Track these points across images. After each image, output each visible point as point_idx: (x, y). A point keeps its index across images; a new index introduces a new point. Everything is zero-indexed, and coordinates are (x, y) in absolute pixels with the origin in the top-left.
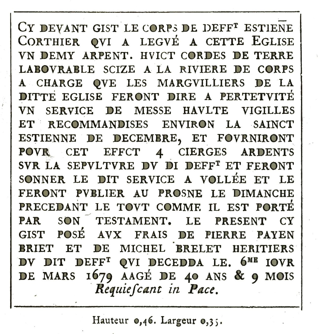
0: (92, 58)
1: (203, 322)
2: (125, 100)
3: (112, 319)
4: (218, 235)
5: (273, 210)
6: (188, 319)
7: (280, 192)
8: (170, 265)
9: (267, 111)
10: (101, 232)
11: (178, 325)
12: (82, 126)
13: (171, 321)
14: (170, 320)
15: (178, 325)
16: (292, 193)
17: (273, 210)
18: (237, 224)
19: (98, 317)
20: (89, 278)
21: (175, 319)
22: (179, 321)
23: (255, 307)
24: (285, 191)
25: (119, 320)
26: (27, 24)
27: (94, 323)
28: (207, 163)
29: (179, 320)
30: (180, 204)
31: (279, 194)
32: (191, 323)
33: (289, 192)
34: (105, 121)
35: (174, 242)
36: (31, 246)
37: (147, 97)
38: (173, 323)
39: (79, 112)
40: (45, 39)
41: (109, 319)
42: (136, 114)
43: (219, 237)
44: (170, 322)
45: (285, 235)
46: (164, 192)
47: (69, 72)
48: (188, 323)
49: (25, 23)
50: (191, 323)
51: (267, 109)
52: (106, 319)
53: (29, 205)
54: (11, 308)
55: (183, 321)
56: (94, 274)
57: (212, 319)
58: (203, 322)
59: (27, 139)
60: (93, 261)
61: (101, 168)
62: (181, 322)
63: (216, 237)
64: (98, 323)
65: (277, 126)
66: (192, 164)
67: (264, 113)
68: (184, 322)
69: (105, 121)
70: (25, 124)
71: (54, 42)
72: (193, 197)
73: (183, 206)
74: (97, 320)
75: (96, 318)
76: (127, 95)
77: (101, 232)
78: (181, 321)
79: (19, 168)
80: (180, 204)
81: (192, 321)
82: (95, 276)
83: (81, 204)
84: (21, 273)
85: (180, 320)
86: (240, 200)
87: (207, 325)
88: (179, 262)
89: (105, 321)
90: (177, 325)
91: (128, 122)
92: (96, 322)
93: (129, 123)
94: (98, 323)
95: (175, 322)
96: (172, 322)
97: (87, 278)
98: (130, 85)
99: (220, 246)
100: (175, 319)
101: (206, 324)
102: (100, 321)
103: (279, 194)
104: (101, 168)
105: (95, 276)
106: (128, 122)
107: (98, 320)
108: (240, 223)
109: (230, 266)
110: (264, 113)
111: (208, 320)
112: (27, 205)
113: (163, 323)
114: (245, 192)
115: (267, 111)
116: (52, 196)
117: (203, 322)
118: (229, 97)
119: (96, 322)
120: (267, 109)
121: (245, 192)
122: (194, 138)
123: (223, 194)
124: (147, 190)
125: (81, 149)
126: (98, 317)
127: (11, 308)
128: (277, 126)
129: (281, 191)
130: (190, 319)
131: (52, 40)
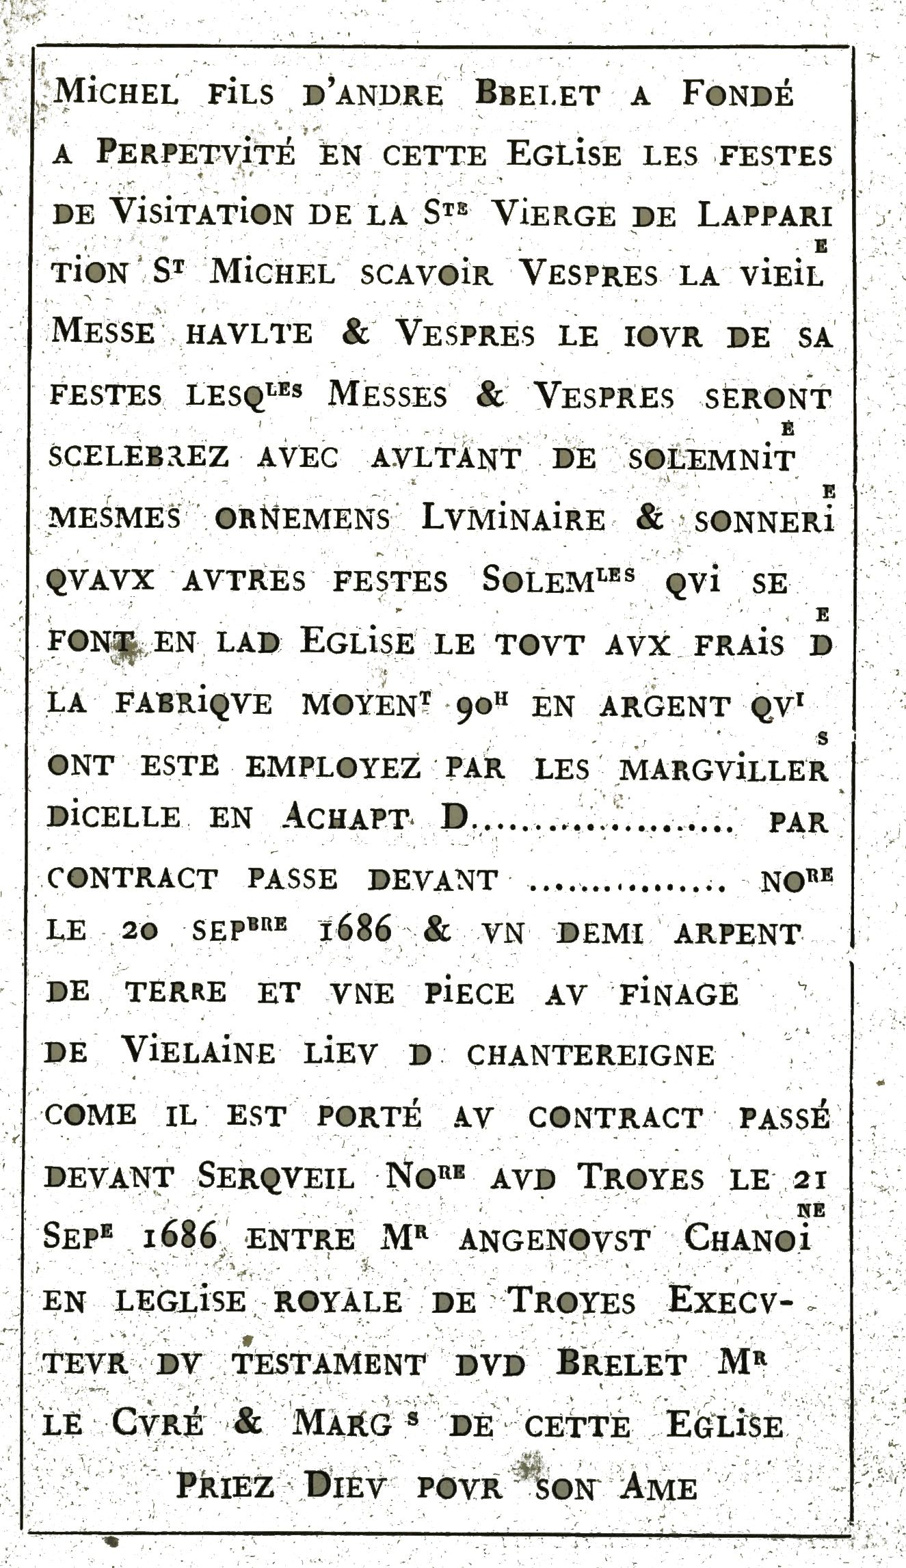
4: (146, 94)
5: (364, 1125)
7: (119, 89)
10: (501, 1172)
12: (94, 1120)
16: (199, 455)
17: (364, 1125)
24: (290, 267)
31: (327, 822)
33: (150, 514)
43: (150, 98)
45: (378, 1364)
61: (266, 341)
66: (65, 987)
76: (231, 926)
77: (501, 1172)
79: (754, 590)
83: (597, 1110)
84: (374, 872)
86: (588, 1394)
98: (226, 646)
103: (326, 820)
104: (266, 341)
118: (185, 154)
122: (234, 1115)
123: (776, 1427)
124: (638, 926)
129: (123, 87)
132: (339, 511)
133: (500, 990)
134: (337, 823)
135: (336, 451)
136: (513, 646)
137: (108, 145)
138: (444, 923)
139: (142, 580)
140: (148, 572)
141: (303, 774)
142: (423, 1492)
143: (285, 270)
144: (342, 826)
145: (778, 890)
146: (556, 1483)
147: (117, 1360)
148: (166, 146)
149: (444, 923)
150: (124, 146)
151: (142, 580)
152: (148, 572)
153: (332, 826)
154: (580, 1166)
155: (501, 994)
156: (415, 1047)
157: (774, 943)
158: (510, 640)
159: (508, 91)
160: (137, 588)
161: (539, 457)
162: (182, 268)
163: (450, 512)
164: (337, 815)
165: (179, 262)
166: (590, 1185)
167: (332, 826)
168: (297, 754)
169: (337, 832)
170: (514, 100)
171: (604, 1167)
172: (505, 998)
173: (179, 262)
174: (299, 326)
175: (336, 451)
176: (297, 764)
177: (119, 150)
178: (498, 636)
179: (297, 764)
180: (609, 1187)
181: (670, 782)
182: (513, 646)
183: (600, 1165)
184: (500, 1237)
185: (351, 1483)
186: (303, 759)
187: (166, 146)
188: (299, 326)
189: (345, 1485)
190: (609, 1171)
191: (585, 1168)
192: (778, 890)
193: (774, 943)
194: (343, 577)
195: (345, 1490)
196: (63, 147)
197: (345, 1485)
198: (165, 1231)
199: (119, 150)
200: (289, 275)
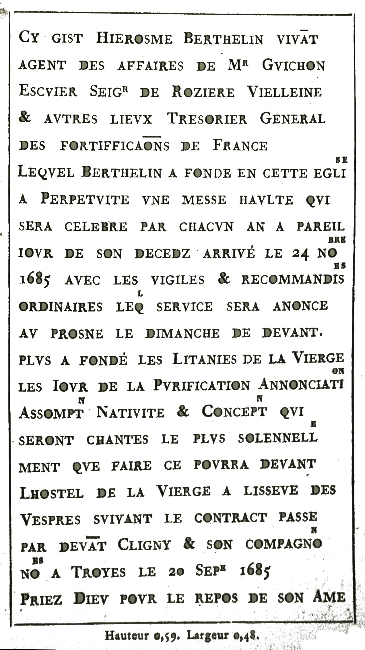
0: (159, 230)
2: (215, 96)
3: (129, 634)
8: (186, 230)
9: (180, 281)
15: (208, 640)
22: (208, 635)
23: (69, 13)
26: (129, 541)
28: (170, 303)
30: (288, 276)
34: (68, 303)
36: (62, 517)
37: (259, 39)
39: (199, 388)
40: (90, 142)
42: (230, 69)
46: (76, 198)
49: (28, 32)
51: (180, 279)
53: (60, 518)
54: (11, 626)
60: (166, 305)
63: (223, 362)
65: (248, 148)
67: (178, 283)
69: (68, 303)
70: (279, 172)
71: (123, 173)
73: (291, 278)
80: (288, 276)
85: (210, 634)
88: (171, 253)
89: (120, 637)
95: (204, 637)
96: (200, 636)
99: (266, 408)
102: (114, 637)
108: (44, 523)
109: (258, 638)
110: (178, 283)
112: (58, 519)
114: (161, 332)
115: (180, 281)
120: (180, 279)
121: (161, 332)
125: (281, 170)
127: (11, 626)
128: (248, 148)
131: (121, 171)
133: (165, 252)
134: (100, 442)
137: (46, 196)
138: (186, 408)
139: (147, 120)
140: (150, 116)
141: (69, 417)
142: (156, 387)
144: (103, 443)
146: (247, 436)
148: (71, 196)
149: (186, 408)
150: (52, 196)
151: (147, 120)
152: (150, 116)
153: (98, 443)
155: (165, 254)
160: (145, 123)
161: (226, 333)
163: (212, 435)
164: (100, 438)
167: (98, 443)
168: (66, 408)
169: (101, 446)
172: (167, 256)
176: (67, 413)
177: (50, 197)
179: (67, 413)
181: (212, 259)
185: (127, 117)
186: (69, 410)
187: (71, 196)
189: (91, 599)
195: (91, 601)
196: (23, 196)
197: (91, 599)
198: (29, 277)
199: (50, 197)
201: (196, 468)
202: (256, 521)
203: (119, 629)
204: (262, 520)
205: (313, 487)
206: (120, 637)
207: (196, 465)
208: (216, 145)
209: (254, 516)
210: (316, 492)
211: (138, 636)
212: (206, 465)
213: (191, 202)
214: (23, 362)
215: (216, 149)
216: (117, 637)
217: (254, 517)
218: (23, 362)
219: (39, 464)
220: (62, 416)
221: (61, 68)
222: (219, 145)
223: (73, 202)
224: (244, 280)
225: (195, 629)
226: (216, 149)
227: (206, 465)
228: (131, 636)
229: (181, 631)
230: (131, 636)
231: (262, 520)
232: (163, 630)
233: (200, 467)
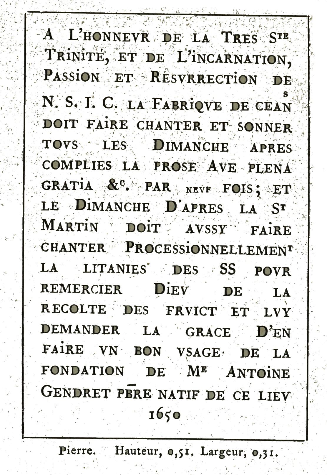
1: (255, 454)
3: (139, 450)
6: (148, 450)
11: (222, 457)
13: (212, 452)
14: (212, 450)
15: (222, 457)
18: (139, 272)
19: (122, 447)
20: (152, 418)
21: (86, 449)
22: (222, 452)
25: (232, 452)
27: (117, 453)
29: (222, 451)
32: (237, 455)
35: (223, 353)
38: (216, 454)
41: (236, 451)
44: (211, 454)
47: (109, 209)
48: (132, 454)
50: (237, 455)
52: (132, 450)
55: (88, 451)
56: (158, 412)
57: (266, 451)
58: (171, 452)
59: (143, 311)
62: (225, 454)
64: (122, 453)
68: (229, 453)
72: (123, 272)
74: (119, 450)
75: (120, 448)
78: (225, 452)
81: (238, 453)
82: (160, 415)
85: (224, 451)
87: (176, 457)
89: (130, 452)
90: (220, 457)
91: (243, 185)
92: (120, 452)
93: (246, 187)
94: (122, 453)
95: (218, 453)
96: (214, 453)
97: (150, 417)
100: (86, 449)
101: (174, 455)
102: (124, 452)
105: (160, 415)
106: (243, 185)
107: (122, 450)
111: (260, 452)
113: (203, 454)
116: (155, 355)
117: (171, 452)
119: (120, 452)
126: (122, 447)
130: (135, 450)
132: (99, 162)
135: (112, 98)
136: (50, 145)
143: (215, 145)
145: (121, 210)
147: (145, 36)
154: (222, 33)
156: (233, 103)
157: (76, 252)
158: (49, 142)
159: (176, 103)
162: (285, 208)
165: (283, 206)
166: (227, 41)
170: (178, 107)
171: (233, 34)
173: (283, 206)
174: (186, 122)
175: (112, 98)
178: (43, 141)
180: (235, 42)
182: (50, 145)
183: (231, 33)
184: (206, 57)
188: (186, 122)
190: (235, 35)
191: (224, 34)
192: (121, 210)
193: (76, 252)
194: (196, 393)
200: (217, 147)
201: (257, 274)
202: (206, 314)
203: (128, 445)
204: (212, 314)
205: (226, 288)
206: (130, 452)
207: (257, 271)
208: (155, 104)
209: (203, 309)
210: (228, 293)
211: (147, 451)
212: (267, 271)
213: (67, 290)
214: (121, 395)
215: (155, 108)
216: (127, 453)
217: (204, 311)
218: (121, 395)
219: (111, 286)
220: (69, 167)
221: (73, 127)
222: (159, 104)
223: (79, 167)
224: (43, 309)
225: (209, 446)
226: (155, 108)
227: (267, 271)
228: (140, 452)
229: (195, 447)
230: (140, 452)
231: (212, 314)
232: (176, 446)
233: (261, 273)
